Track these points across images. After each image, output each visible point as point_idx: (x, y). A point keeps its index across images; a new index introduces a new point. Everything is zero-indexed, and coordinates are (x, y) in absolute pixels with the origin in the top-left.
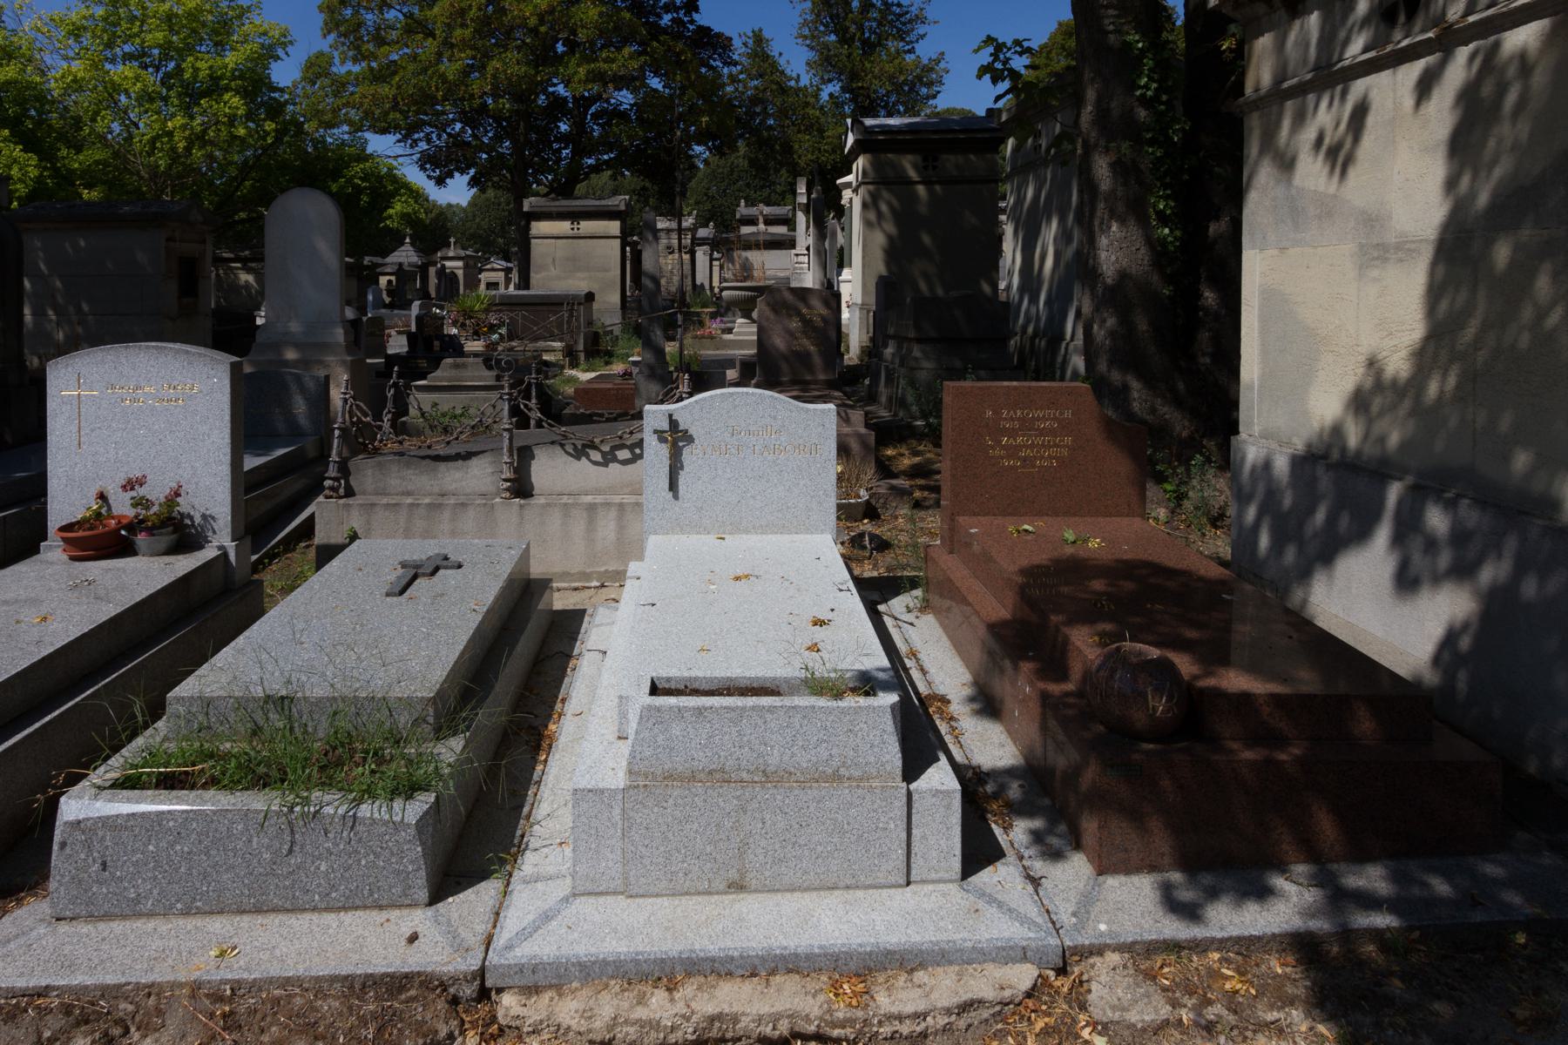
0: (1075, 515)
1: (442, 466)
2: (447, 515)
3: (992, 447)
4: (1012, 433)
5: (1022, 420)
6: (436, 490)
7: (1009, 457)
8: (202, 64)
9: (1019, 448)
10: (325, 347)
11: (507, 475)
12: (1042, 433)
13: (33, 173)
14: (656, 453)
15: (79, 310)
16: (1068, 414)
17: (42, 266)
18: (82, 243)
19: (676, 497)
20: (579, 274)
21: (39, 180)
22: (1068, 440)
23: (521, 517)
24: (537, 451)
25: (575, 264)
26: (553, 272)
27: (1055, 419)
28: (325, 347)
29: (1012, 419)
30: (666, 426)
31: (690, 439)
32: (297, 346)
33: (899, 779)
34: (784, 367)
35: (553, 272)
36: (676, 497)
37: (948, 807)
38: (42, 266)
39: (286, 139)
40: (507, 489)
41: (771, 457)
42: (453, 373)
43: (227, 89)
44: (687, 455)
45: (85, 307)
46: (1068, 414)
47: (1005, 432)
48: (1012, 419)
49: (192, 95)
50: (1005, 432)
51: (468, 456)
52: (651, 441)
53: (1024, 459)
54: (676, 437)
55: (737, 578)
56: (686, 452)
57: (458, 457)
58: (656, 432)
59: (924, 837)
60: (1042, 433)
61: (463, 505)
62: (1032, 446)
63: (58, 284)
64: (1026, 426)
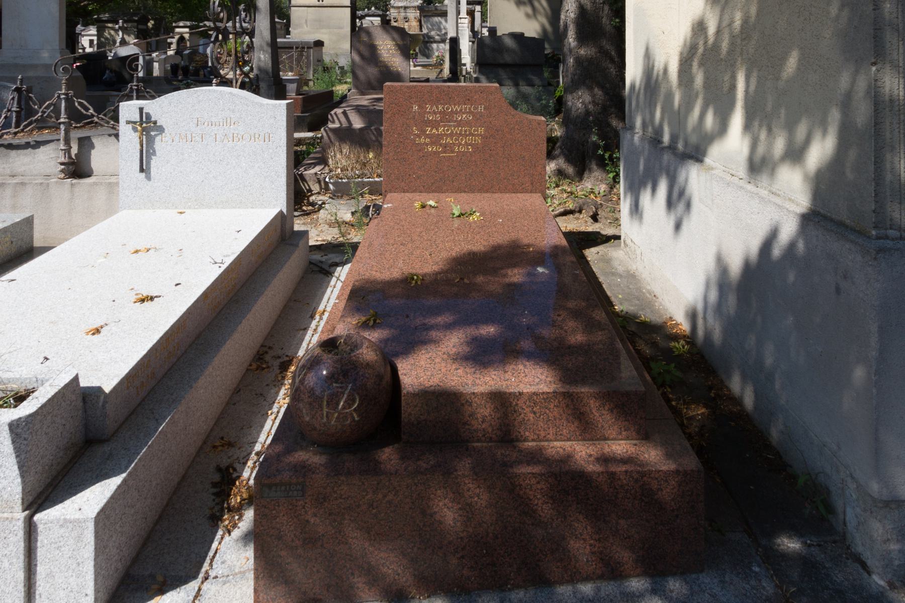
0: (487, 192)
1: (13, 153)
2: (8, 192)
3: (419, 136)
4: (435, 125)
5: (443, 113)
6: (8, 172)
7: (432, 143)
9: (440, 137)
11: (63, 160)
12: (459, 124)
14: (129, 137)
16: (481, 109)
19: (148, 178)
20: (324, 31)
22: (481, 130)
23: (72, 192)
24: (94, 140)
25: (320, 24)
26: (306, 28)
27: (470, 112)
29: (435, 113)
30: (137, 118)
31: (161, 129)
33: (18, 506)
35: (306, 28)
36: (148, 178)
37: (79, 538)
40: (62, 171)
41: (231, 144)
44: (160, 144)
46: (481, 109)
47: (429, 123)
48: (435, 113)
50: (429, 123)
51: (38, 145)
52: (124, 129)
53: (445, 146)
54: (148, 127)
55: (137, 252)
56: (158, 139)
57: (27, 146)
58: (128, 122)
59: (50, 575)
60: (459, 124)
61: (23, 184)
62: (451, 135)
64: (446, 117)
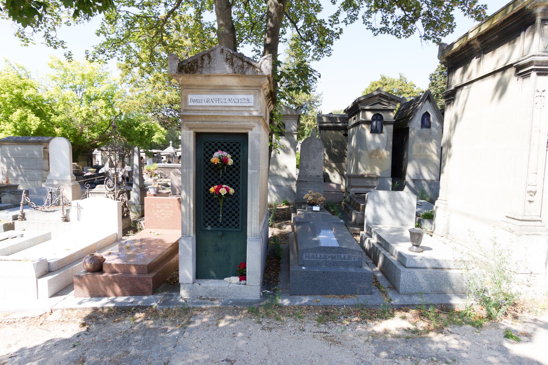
4: (159, 209)
5: (161, 206)
8: (92, 91)
10: (64, 181)
13: (38, 123)
15: (20, 168)
17: (9, 154)
18: (20, 148)
21: (40, 125)
28: (64, 181)
32: (58, 180)
34: (178, 190)
38: (9, 154)
39: (296, 76)
42: (100, 189)
43: (100, 98)
44: (82, 212)
45: (21, 167)
46: (172, 205)
47: (157, 209)
49: (90, 99)
63: (13, 160)
